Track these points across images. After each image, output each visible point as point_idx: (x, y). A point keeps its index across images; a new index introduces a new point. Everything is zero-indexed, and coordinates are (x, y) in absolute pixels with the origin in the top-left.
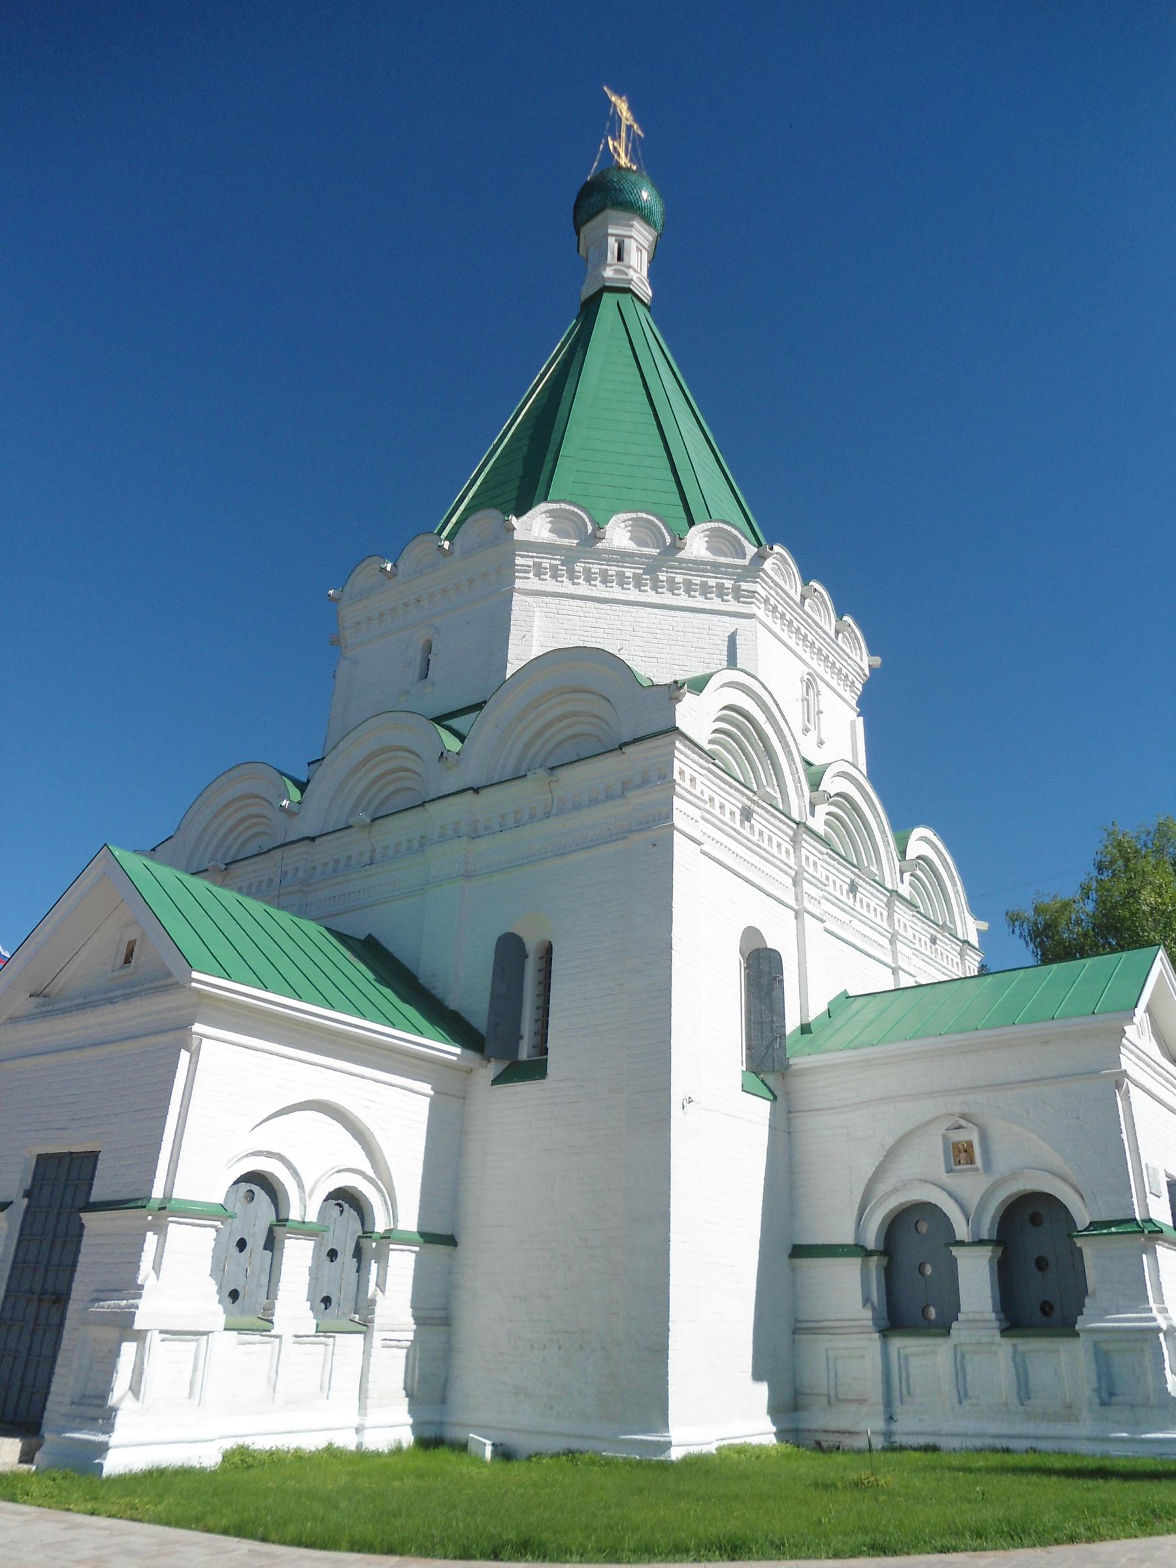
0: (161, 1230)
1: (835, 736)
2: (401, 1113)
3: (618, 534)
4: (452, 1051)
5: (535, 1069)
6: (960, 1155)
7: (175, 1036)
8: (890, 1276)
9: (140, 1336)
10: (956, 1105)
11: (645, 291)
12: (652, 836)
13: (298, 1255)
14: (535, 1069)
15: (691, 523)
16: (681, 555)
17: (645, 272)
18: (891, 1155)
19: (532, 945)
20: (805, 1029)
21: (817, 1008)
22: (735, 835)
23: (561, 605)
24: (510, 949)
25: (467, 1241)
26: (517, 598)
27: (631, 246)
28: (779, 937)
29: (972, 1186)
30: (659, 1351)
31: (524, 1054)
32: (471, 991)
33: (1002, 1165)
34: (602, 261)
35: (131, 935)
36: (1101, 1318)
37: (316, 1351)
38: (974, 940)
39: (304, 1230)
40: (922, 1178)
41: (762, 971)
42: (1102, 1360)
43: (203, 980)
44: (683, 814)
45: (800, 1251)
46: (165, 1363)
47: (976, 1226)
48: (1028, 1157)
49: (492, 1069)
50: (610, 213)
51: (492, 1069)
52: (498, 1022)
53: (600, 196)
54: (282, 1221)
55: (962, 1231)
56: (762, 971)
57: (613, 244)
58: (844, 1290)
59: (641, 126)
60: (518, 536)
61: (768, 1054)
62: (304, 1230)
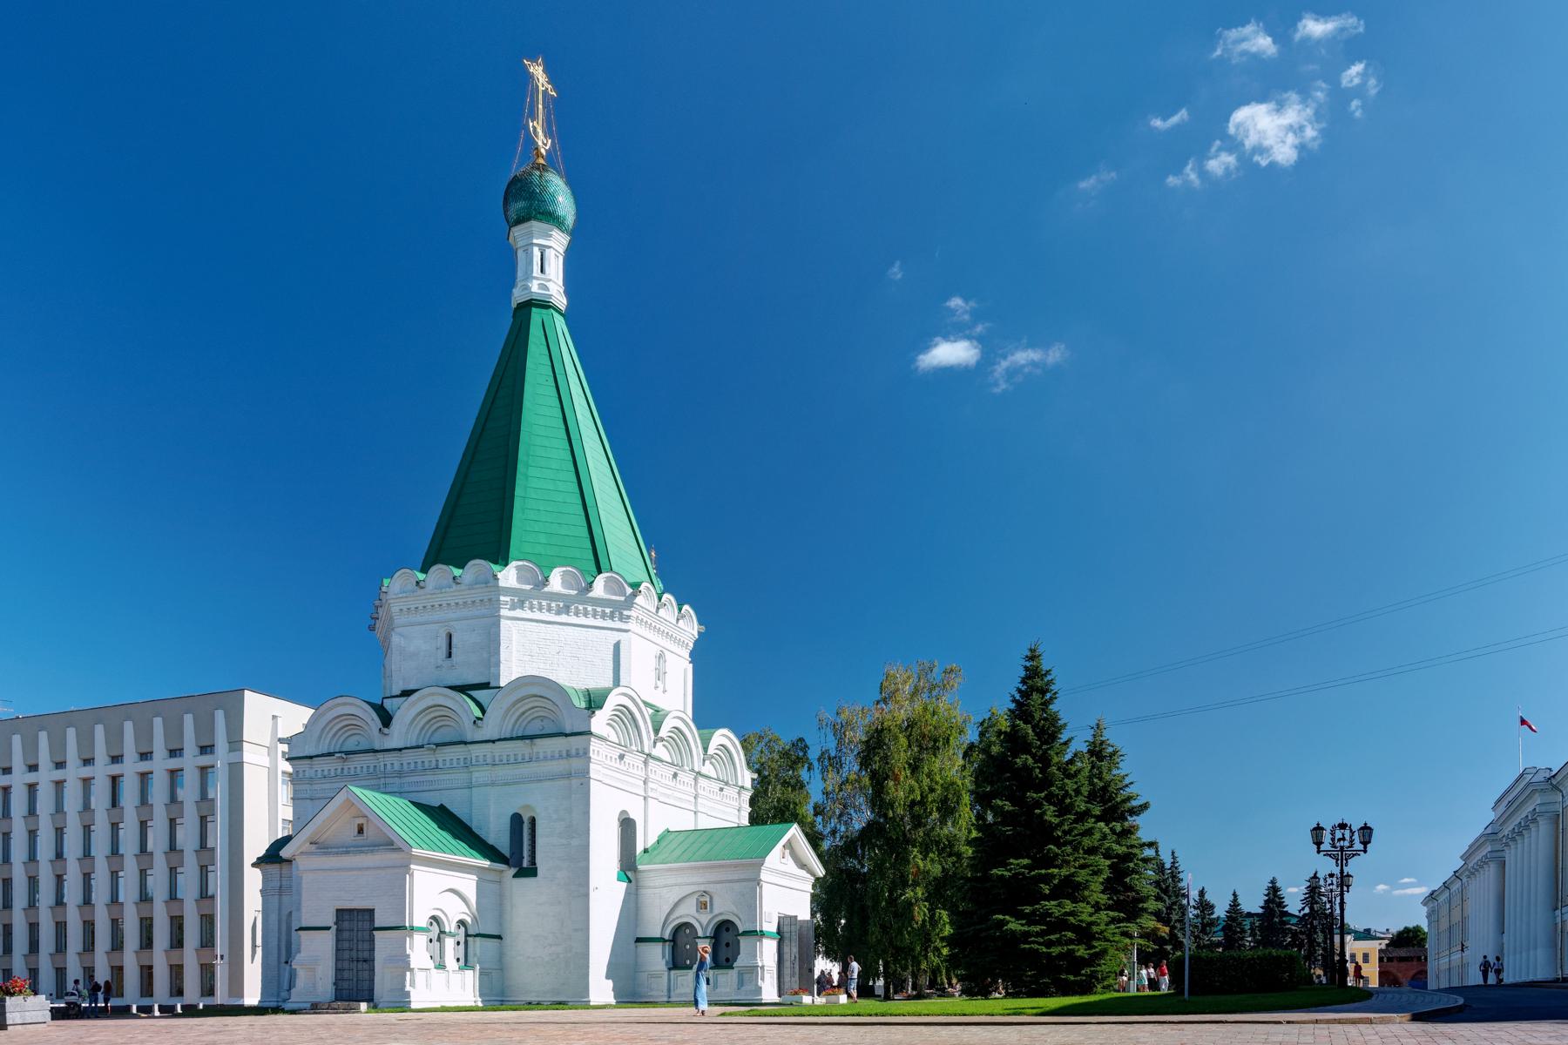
0: (411, 937)
1: (675, 692)
2: (468, 885)
3: (556, 582)
4: (486, 863)
5: (531, 872)
6: (702, 906)
7: (405, 868)
8: (674, 949)
9: (411, 970)
10: (702, 888)
11: (561, 301)
12: (582, 778)
13: (449, 943)
14: (531, 872)
15: (600, 572)
16: (591, 595)
17: (560, 282)
18: (676, 905)
19: (526, 819)
20: (646, 851)
21: (652, 840)
22: (617, 770)
23: (537, 643)
24: (516, 820)
25: (507, 939)
26: (503, 622)
27: (550, 254)
28: (636, 815)
29: (705, 918)
30: (587, 975)
31: (525, 864)
32: (501, 840)
33: (716, 912)
34: (529, 276)
35: (361, 821)
36: (741, 961)
37: (459, 976)
38: (748, 784)
39: (451, 935)
40: (688, 912)
41: (627, 826)
42: (740, 974)
43: (416, 851)
44: (595, 770)
45: (639, 940)
46: (420, 977)
47: (704, 929)
48: (723, 908)
49: (513, 871)
50: (535, 225)
51: (513, 871)
52: (513, 853)
53: (525, 202)
54: (442, 932)
55: (700, 934)
56: (627, 826)
57: (536, 252)
58: (656, 957)
59: (555, 88)
60: (502, 584)
61: (629, 865)
62: (451, 935)
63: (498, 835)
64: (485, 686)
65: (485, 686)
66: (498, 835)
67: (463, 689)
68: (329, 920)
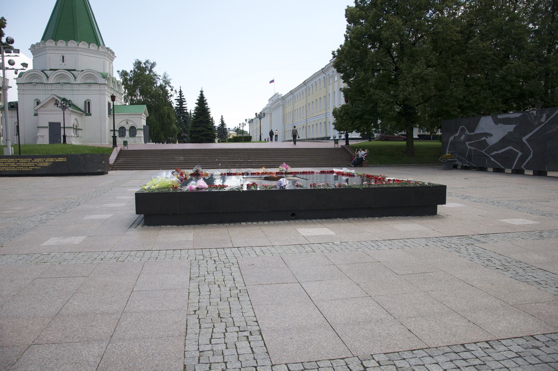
5: (91, 115)
40: (124, 124)
48: (131, 124)
63: (81, 106)
64: (75, 70)
65: (75, 70)
66: (81, 106)
67: (69, 70)
68: (47, 125)
